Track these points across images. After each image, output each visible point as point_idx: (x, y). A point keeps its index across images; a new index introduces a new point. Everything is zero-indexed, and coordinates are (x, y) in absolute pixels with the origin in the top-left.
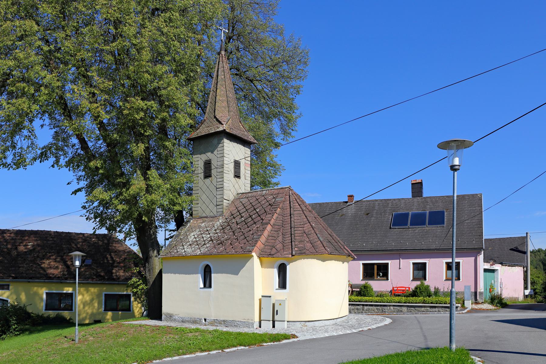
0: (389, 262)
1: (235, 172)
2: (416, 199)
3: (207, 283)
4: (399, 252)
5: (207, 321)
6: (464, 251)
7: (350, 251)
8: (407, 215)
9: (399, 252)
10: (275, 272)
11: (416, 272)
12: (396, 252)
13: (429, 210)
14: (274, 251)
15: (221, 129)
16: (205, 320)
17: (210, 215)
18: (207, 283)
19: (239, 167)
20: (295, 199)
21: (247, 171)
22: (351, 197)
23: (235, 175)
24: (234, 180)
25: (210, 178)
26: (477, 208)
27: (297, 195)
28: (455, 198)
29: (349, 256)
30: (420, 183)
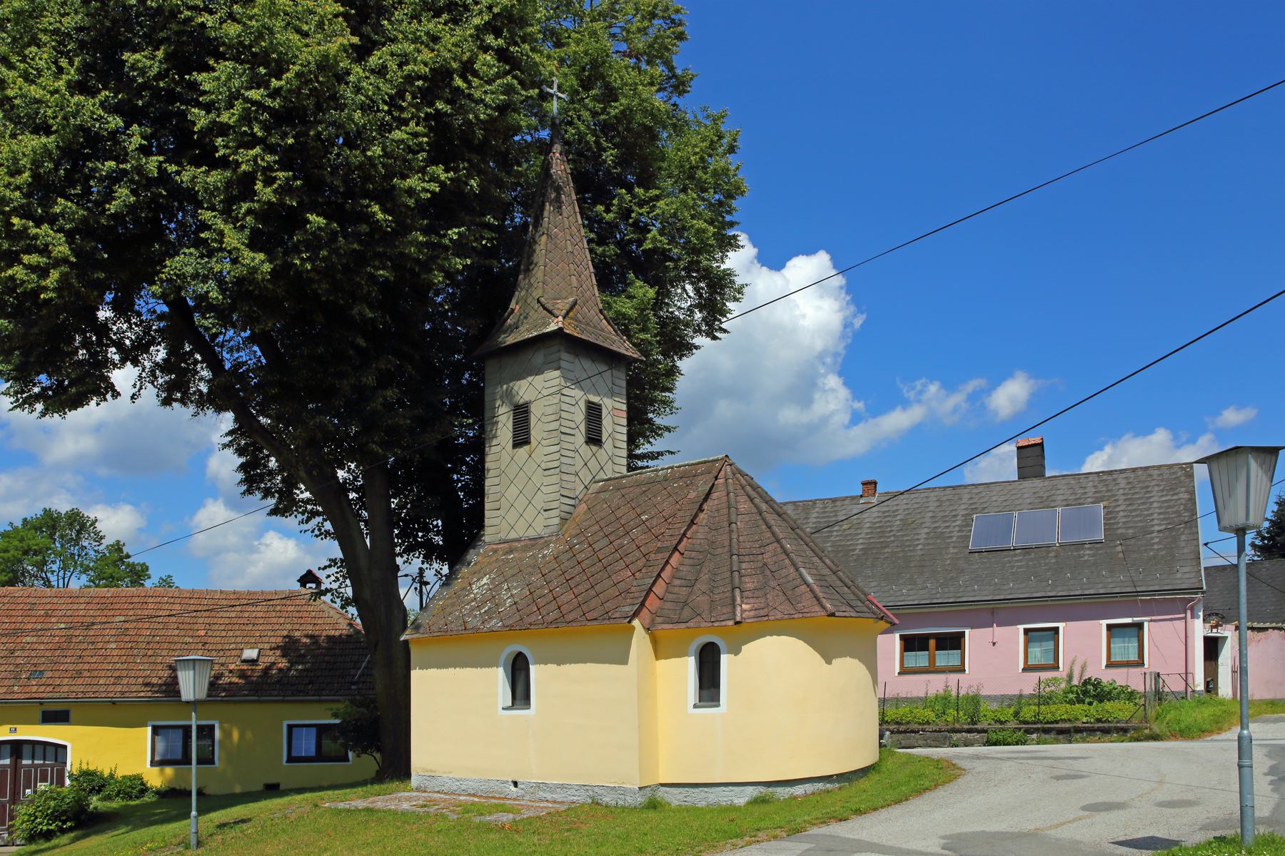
0: (1061, 625)
1: (589, 430)
2: (1027, 484)
3: (520, 693)
4: (991, 606)
5: (519, 786)
6: (1079, 601)
7: (884, 609)
8: (201, 812)
9: (991, 606)
10: (689, 666)
11: (1208, 663)
12: (971, 607)
13: (1061, 506)
14: (687, 612)
15: (552, 327)
16: (515, 784)
17: (526, 535)
18: (520, 693)
19: (600, 417)
20: (741, 485)
21: (619, 429)
22: (870, 485)
23: (589, 438)
24: (586, 451)
25: (526, 448)
26: (1181, 496)
27: (743, 475)
28: (194, 813)
29: (882, 618)
30: (1038, 444)
